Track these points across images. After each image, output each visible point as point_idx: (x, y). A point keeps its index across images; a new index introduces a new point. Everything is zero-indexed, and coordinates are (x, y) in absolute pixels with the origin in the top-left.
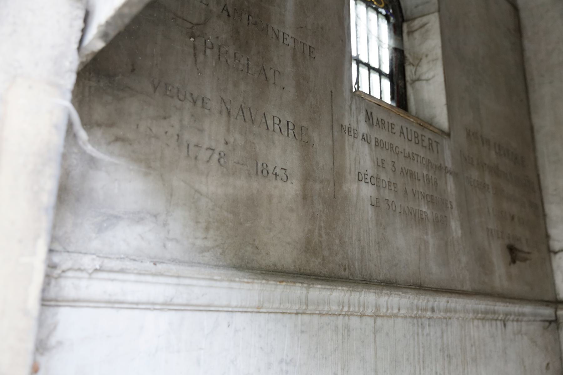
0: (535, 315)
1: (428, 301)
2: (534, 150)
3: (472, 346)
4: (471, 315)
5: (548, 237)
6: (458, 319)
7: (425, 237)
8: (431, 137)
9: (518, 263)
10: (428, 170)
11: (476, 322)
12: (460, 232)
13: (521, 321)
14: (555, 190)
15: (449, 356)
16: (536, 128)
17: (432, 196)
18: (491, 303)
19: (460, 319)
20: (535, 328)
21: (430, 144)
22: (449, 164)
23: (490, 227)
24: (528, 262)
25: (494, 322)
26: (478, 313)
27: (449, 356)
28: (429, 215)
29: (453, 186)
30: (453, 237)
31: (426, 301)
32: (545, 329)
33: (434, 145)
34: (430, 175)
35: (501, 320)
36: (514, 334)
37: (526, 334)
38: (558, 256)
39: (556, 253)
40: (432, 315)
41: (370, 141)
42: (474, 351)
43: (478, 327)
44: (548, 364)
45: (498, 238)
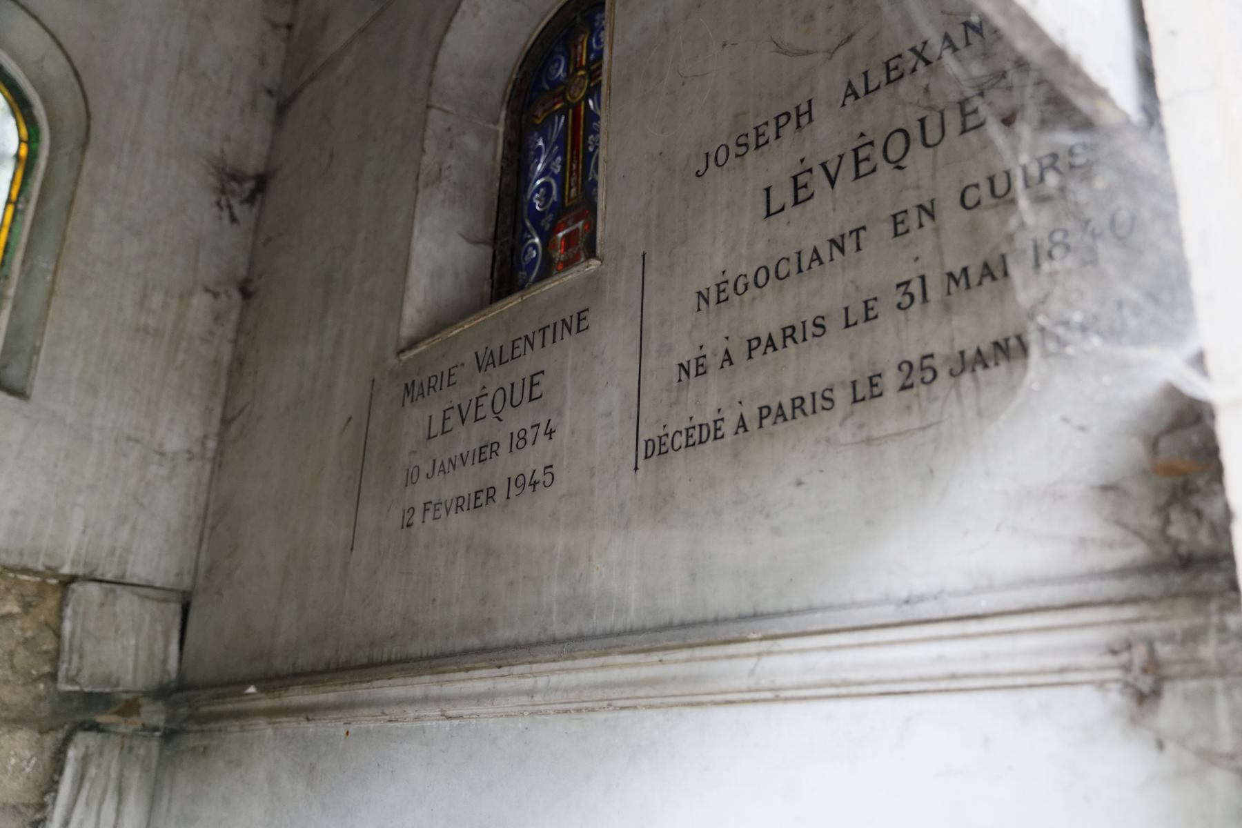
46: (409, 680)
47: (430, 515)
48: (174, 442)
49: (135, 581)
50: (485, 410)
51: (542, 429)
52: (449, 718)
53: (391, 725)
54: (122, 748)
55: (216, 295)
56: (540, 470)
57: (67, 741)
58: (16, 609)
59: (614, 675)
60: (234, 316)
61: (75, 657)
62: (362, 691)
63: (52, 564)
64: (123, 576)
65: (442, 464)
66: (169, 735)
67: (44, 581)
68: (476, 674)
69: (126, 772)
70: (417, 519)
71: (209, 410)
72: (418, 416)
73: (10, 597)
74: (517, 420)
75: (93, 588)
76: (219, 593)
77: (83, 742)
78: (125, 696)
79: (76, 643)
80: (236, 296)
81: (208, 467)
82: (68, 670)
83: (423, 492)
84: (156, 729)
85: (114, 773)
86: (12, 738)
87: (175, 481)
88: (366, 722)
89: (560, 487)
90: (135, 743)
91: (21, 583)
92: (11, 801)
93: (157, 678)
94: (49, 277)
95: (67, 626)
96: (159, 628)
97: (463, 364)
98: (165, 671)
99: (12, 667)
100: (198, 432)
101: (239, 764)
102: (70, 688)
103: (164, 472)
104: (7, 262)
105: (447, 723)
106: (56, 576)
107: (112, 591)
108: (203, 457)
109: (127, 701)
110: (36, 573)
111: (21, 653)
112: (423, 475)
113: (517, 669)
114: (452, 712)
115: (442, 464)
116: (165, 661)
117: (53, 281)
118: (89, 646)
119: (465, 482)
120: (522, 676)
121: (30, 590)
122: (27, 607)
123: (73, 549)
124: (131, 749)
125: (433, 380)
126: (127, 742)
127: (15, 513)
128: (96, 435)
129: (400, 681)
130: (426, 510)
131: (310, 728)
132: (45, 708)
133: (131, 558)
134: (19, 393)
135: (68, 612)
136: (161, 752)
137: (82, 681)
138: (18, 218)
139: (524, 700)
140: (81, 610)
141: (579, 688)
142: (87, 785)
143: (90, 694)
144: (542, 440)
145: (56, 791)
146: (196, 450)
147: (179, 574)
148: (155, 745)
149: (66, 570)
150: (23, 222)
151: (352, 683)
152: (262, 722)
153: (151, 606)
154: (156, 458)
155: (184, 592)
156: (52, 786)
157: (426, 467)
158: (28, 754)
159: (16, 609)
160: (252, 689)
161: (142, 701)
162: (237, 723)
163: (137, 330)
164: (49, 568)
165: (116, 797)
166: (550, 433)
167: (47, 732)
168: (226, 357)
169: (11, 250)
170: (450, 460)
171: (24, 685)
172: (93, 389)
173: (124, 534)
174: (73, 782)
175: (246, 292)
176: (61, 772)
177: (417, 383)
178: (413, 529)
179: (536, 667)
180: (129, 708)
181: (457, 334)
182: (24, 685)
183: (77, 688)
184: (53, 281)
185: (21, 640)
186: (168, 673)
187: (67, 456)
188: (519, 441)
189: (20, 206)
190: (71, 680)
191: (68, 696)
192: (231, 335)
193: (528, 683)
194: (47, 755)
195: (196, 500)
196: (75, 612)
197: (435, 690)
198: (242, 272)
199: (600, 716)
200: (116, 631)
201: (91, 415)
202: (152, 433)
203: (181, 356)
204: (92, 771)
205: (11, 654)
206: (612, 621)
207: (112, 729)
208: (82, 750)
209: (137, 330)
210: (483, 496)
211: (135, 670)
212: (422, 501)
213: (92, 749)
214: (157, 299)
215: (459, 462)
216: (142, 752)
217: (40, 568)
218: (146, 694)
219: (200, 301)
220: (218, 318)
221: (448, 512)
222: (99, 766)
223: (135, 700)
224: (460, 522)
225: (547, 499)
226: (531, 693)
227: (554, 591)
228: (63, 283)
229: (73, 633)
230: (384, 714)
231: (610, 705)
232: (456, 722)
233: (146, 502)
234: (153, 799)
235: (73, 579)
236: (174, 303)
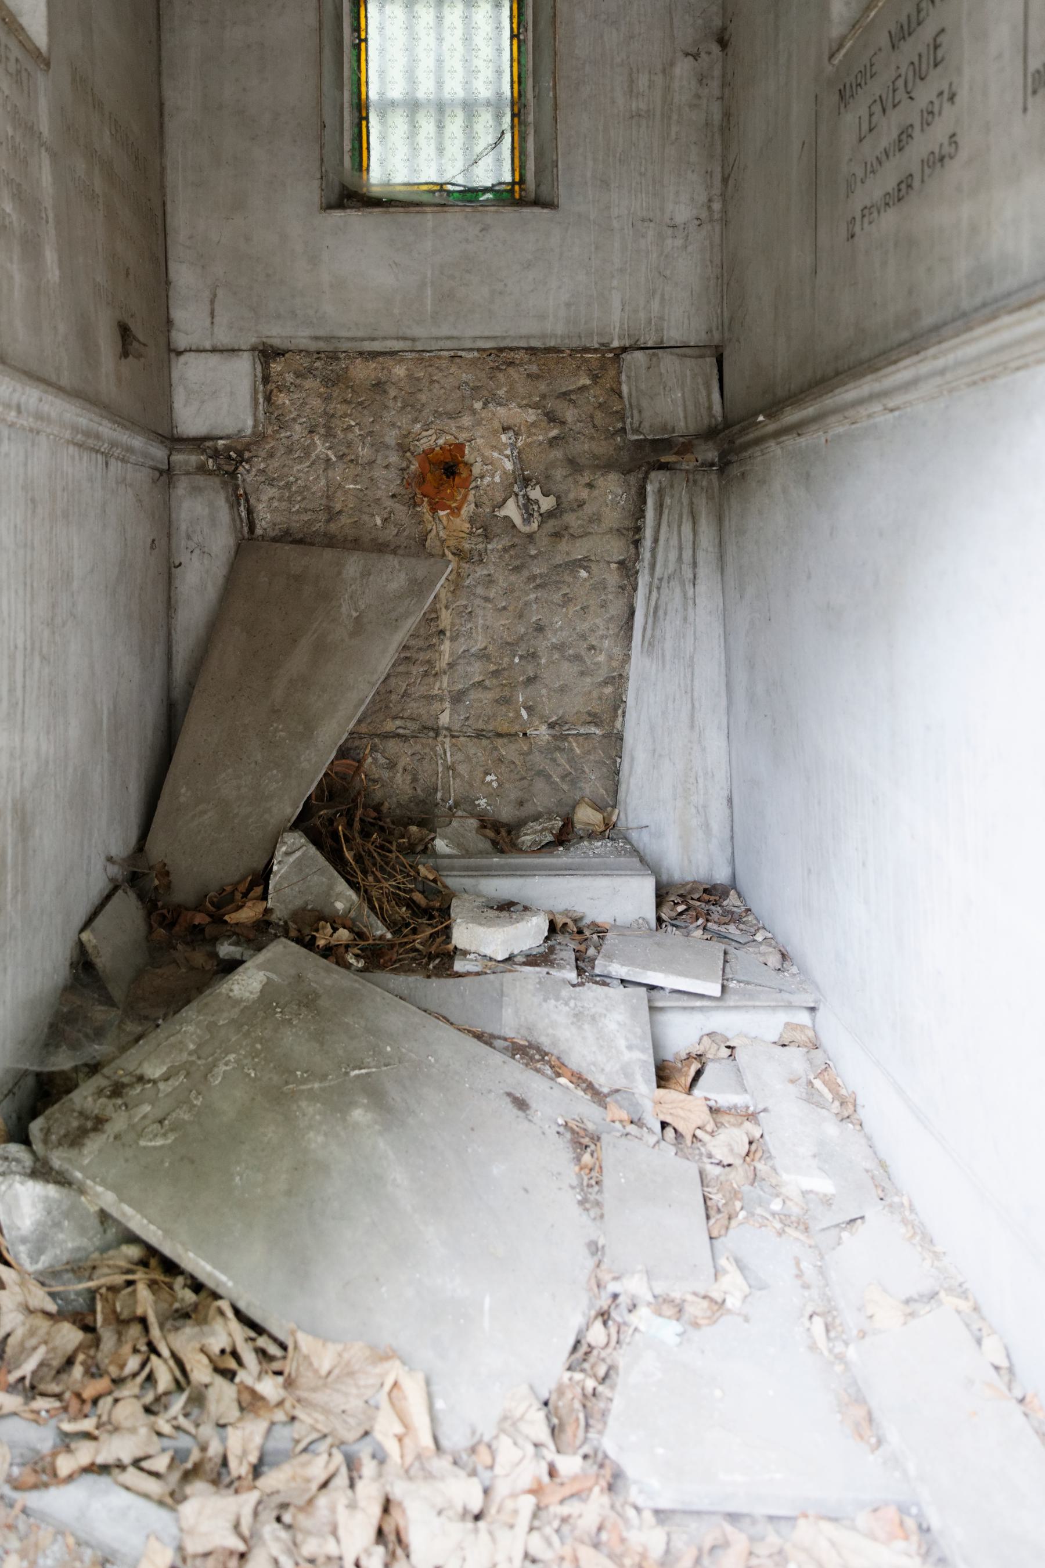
0: (146, 455)
1: (14, 390)
2: (162, 150)
3: (64, 490)
4: (68, 434)
5: (169, 322)
6: (48, 436)
7: (9, 265)
8: (19, 57)
9: (131, 357)
10: (15, 129)
11: (71, 448)
12: (57, 273)
13: (127, 462)
14: (191, 237)
15: (33, 500)
16: (169, 105)
17: (19, 185)
18: (97, 419)
19: (52, 437)
20: (142, 477)
21: (19, 72)
22: (44, 126)
23: (99, 279)
24: (142, 360)
25: (94, 455)
26: (78, 433)
27: (33, 500)
28: (16, 224)
29: (50, 178)
30: (48, 281)
31: (11, 389)
32: (154, 481)
33: (24, 74)
34: (18, 140)
35: (103, 453)
36: (117, 483)
37: (131, 485)
38: (182, 359)
39: (179, 353)
40: (15, 420)
41: (926, 75)
42: (65, 499)
43: (73, 458)
44: (153, 541)
45: (108, 304)
46: (858, 383)
47: (866, 220)
48: (683, 213)
49: (672, 344)
50: (901, 94)
51: (946, 96)
52: (892, 410)
53: (853, 426)
54: (688, 481)
55: (696, 57)
56: (946, 141)
57: (645, 479)
58: (588, 382)
59: (1006, 336)
60: (717, 72)
61: (635, 412)
62: (829, 401)
63: (605, 341)
64: (662, 342)
65: (872, 165)
66: (723, 465)
67: (603, 356)
68: (902, 364)
69: (694, 500)
70: (857, 229)
71: (709, 174)
72: (852, 119)
73: (581, 373)
74: (925, 94)
75: (639, 355)
76: (738, 341)
77: (655, 482)
78: (681, 440)
79: (634, 402)
80: (715, 48)
81: (718, 228)
82: (631, 424)
83: (860, 199)
84: (712, 464)
85: (685, 501)
86: (605, 480)
87: (690, 249)
88: (837, 428)
89: (963, 155)
90: (698, 477)
91: (587, 361)
92: (615, 526)
93: (706, 422)
94: (551, 94)
95: (625, 389)
96: (700, 380)
97: (880, 50)
98: (711, 416)
99: (594, 426)
100: (703, 198)
101: (764, 482)
102: (636, 437)
103: (679, 242)
104: (355, 111)
105: (890, 416)
106: (611, 351)
107: (654, 354)
108: (711, 221)
109: (683, 443)
110: (596, 351)
111: (599, 415)
112: (858, 180)
113: (932, 351)
114: (891, 404)
115: (872, 165)
116: (710, 408)
117: (555, 97)
118: (645, 403)
119: (887, 180)
120: (935, 357)
121: (595, 365)
122: (595, 378)
123: (618, 325)
124: (695, 482)
125: (859, 76)
126: (691, 476)
127: (568, 305)
128: (615, 224)
129: (851, 385)
130: (863, 216)
131: (803, 441)
132: (625, 457)
133: (665, 325)
134: (550, 205)
135: (623, 377)
136: (720, 482)
137: (644, 431)
138: (523, 49)
139: (938, 380)
140: (633, 374)
141: (978, 358)
142: (666, 511)
143: (654, 442)
144: (946, 105)
145: (644, 517)
146: (704, 215)
147: (709, 331)
148: (714, 477)
149: (616, 344)
150: (527, 50)
151: (821, 396)
152: (772, 443)
153: (689, 362)
154: (670, 231)
155: (717, 347)
156: (641, 514)
157: (860, 173)
158: (620, 491)
159: (588, 382)
160: (761, 418)
161: (696, 442)
162: (757, 448)
163: (632, 117)
164: (603, 345)
165: (690, 519)
166: (952, 98)
167: (629, 472)
168: (717, 117)
169: (523, 80)
170: (877, 158)
171: (606, 439)
172: (605, 184)
173: (655, 305)
174: (655, 509)
175: (723, 43)
176: (645, 503)
177: (848, 86)
178: (856, 238)
179: (945, 346)
180: (685, 448)
181: (875, 16)
182: (606, 439)
183: (642, 437)
184: (555, 97)
185: (596, 405)
186: (714, 416)
187: (597, 248)
188: (929, 114)
189: (522, 37)
190: (636, 431)
191: (639, 445)
192: (717, 93)
193: (940, 363)
194: (633, 491)
195: (711, 262)
196: (628, 377)
197: (877, 387)
198: (717, 22)
199: (1001, 382)
200: (664, 388)
201: (608, 208)
202: (662, 210)
203: (674, 129)
204: (668, 501)
205: (592, 417)
206: (1010, 282)
207: (678, 466)
208: (657, 485)
209: (632, 117)
210: (903, 186)
211: (686, 418)
212: (860, 208)
213: (664, 484)
214: (643, 81)
215: (884, 158)
216: (705, 483)
217: (597, 346)
218: (698, 436)
219: (683, 68)
220: (702, 79)
221: (879, 212)
222: (672, 496)
223: (690, 442)
224: (889, 220)
225: (955, 172)
226: (942, 372)
227: (963, 265)
228: (562, 96)
229: (630, 394)
230: (846, 418)
231: (1005, 369)
232: (896, 413)
233: (668, 273)
234: (720, 520)
235: (624, 349)
236: (659, 80)
